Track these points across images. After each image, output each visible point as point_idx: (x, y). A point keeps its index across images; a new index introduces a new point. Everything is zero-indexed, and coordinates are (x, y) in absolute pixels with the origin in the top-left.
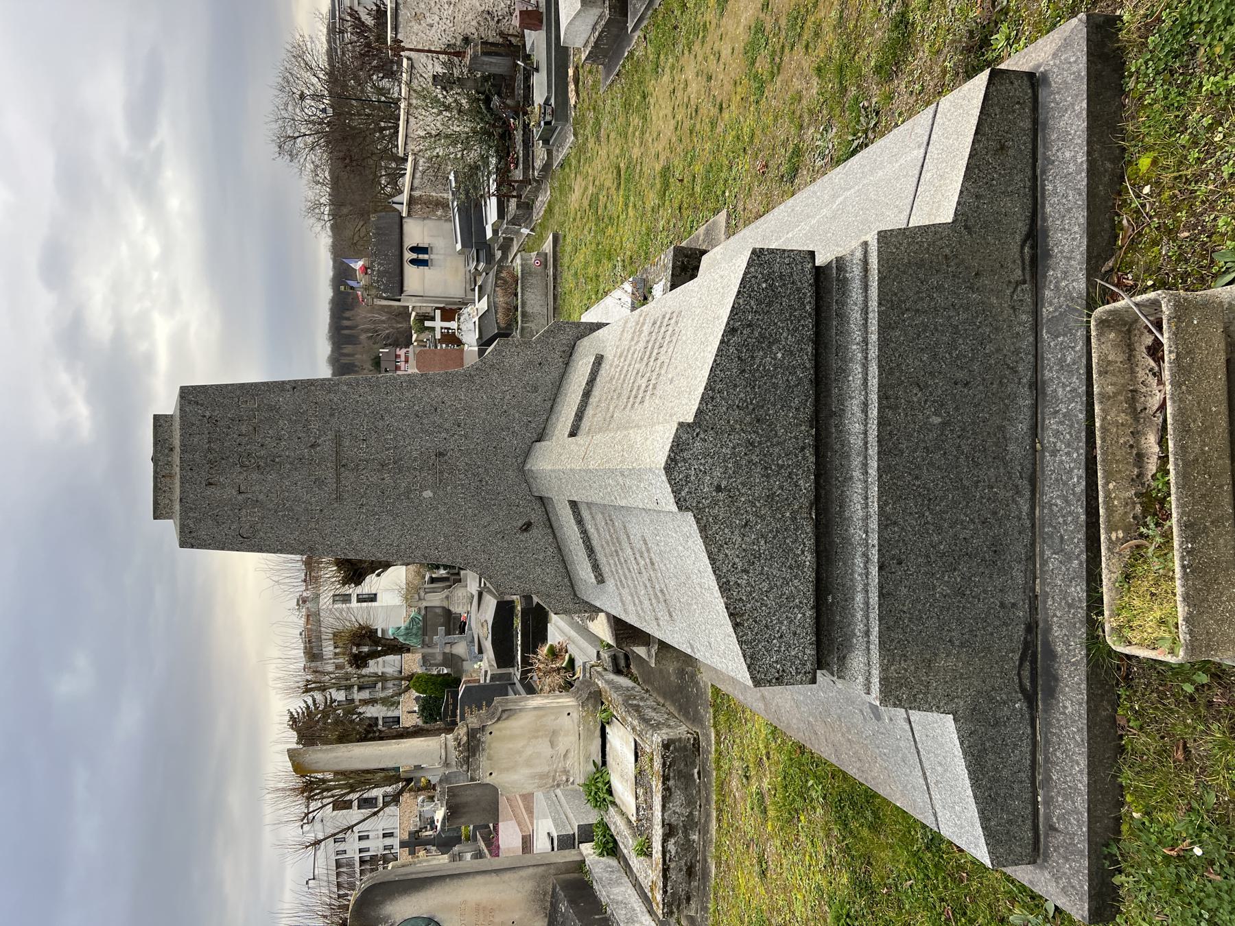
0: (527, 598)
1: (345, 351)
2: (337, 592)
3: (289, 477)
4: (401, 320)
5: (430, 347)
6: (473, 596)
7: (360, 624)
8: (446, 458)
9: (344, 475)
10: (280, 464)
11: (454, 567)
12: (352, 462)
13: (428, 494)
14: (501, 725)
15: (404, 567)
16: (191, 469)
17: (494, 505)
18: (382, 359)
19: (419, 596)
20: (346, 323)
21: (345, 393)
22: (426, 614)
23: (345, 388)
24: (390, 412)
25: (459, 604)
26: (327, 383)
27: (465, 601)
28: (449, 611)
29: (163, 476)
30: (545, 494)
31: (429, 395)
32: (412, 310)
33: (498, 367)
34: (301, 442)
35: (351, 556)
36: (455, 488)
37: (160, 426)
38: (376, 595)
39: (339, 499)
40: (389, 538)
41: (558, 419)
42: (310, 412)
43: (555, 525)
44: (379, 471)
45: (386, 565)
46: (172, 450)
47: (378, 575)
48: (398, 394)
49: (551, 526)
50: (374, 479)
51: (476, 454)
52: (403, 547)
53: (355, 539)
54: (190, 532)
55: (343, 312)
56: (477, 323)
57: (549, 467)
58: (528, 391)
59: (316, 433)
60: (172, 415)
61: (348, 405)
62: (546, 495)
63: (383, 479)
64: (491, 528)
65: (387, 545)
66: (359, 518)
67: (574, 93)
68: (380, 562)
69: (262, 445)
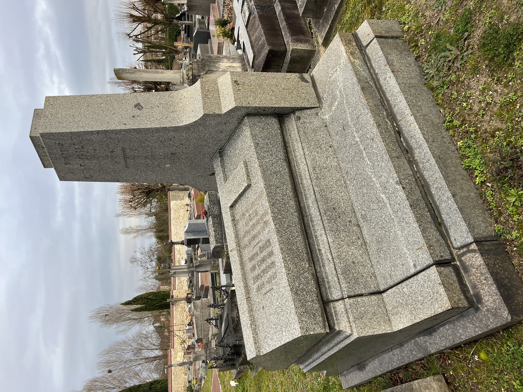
14: (207, 75)
21: (124, 134)
24: (148, 141)
67: (235, 252)
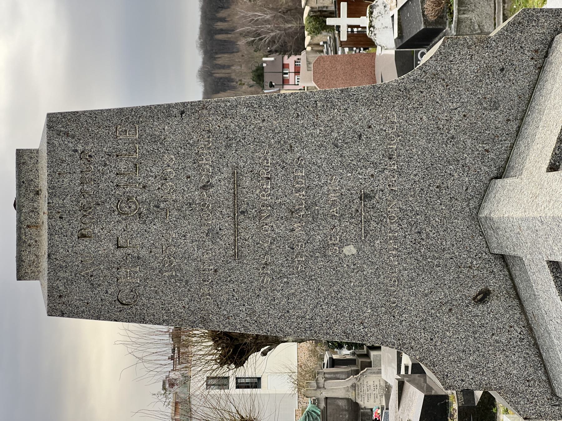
0: (468, 394)
1: (219, 62)
2: (214, 374)
3: (176, 227)
4: (290, 18)
5: (327, 53)
6: (388, 388)
7: (242, 417)
8: (374, 201)
9: (243, 225)
10: (166, 210)
11: (361, 346)
12: (254, 207)
13: (350, 250)
15: (295, 344)
16: (61, 218)
17: (438, 266)
18: (265, 71)
19: (317, 383)
20: (220, 25)
21: (244, 117)
22: (326, 408)
23: (245, 111)
24: (301, 141)
25: (369, 396)
26: (223, 105)
27: (377, 392)
28: (357, 404)
29: (28, 226)
30: (508, 251)
31: (351, 117)
32: (306, 4)
33: (443, 76)
34: (191, 182)
35: (222, 329)
36: (386, 242)
37: (24, 163)
38: (259, 379)
39: (237, 256)
40: (301, 309)
41: (528, 146)
42: (202, 144)
43: (524, 294)
44: (287, 219)
45: (275, 342)
46: (37, 193)
47: (264, 354)
48: (311, 116)
49: (518, 296)
50: (281, 230)
51: (413, 196)
52: (318, 320)
53: (258, 308)
54: (60, 296)
55: (218, 12)
56: (396, 17)
57: (519, 214)
58: (485, 109)
59: (208, 171)
60: (37, 151)
61: (248, 133)
62: (512, 253)
63: (293, 230)
64: (434, 297)
65: (298, 317)
66: (263, 281)
68: (266, 337)
69: (144, 187)
